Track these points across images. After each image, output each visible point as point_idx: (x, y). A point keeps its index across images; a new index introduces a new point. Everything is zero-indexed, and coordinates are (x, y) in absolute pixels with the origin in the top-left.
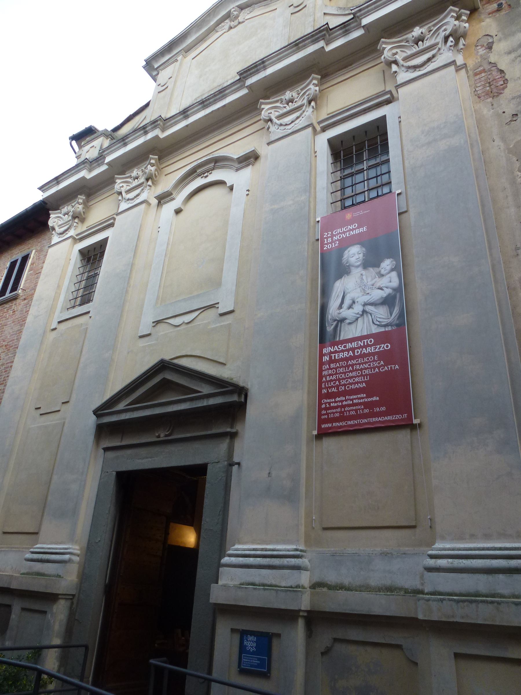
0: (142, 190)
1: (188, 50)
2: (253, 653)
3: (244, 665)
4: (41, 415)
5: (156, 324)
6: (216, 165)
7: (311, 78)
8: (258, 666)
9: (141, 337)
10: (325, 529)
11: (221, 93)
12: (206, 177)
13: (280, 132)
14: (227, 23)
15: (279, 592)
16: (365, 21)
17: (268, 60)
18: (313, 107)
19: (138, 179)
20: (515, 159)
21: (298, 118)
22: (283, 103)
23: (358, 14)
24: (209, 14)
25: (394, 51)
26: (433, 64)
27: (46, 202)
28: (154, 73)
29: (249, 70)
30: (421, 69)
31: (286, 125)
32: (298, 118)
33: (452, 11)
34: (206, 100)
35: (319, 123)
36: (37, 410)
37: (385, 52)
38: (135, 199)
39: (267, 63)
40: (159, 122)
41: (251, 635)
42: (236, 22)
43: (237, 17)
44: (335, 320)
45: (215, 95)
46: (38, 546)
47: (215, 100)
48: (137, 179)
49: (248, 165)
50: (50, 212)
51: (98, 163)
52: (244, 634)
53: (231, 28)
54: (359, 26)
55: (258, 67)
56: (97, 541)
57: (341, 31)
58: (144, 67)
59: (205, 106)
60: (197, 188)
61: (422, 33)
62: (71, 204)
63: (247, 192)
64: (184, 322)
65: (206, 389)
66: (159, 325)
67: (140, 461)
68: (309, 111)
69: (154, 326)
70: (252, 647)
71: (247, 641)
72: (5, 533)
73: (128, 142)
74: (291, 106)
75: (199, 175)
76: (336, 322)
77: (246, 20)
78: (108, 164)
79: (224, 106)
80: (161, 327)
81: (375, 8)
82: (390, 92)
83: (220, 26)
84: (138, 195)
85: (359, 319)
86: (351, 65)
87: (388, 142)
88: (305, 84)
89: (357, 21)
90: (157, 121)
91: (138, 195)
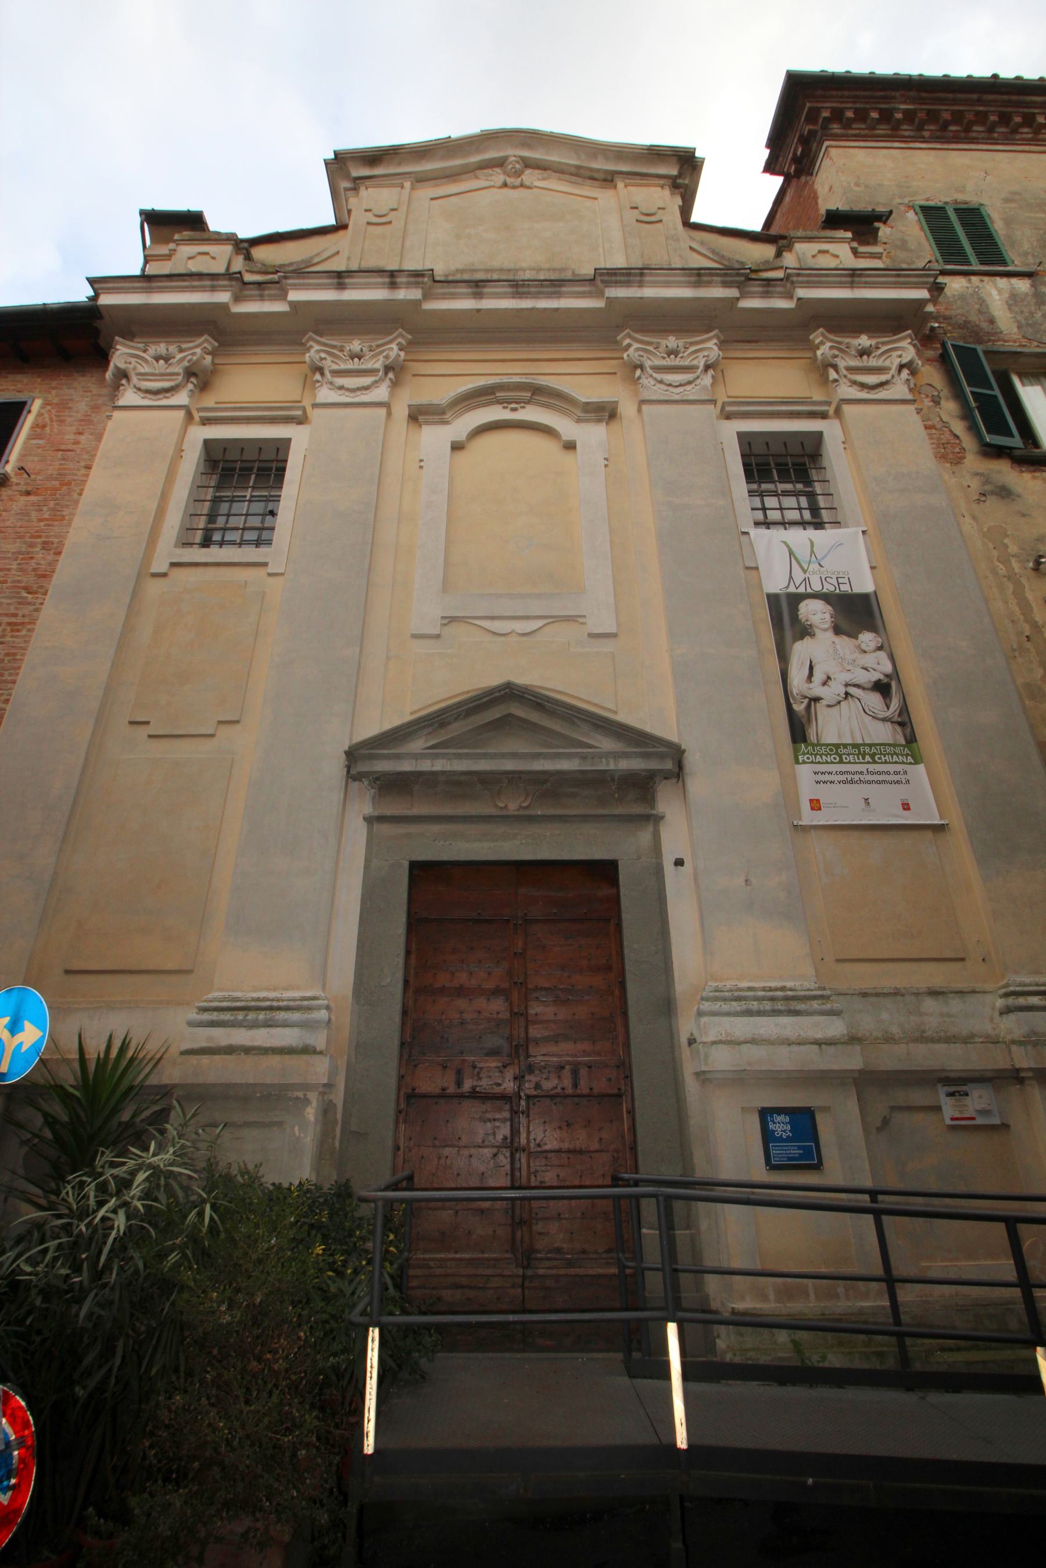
0: (376, 382)
1: (421, 179)
2: (788, 1139)
4: (150, 736)
7: (396, 334)
8: (801, 1157)
14: (498, 177)
16: (802, 293)
19: (362, 360)
21: (689, 383)
23: (795, 279)
24: (471, 142)
28: (345, 184)
31: (670, 385)
32: (689, 383)
33: (401, 335)
37: (312, 351)
38: (359, 393)
39: (647, 278)
41: (779, 1115)
42: (518, 182)
43: (518, 174)
44: (806, 697)
47: (539, 293)
53: (505, 185)
54: (789, 296)
55: (631, 278)
58: (327, 163)
59: (518, 293)
61: (871, 346)
62: (179, 342)
63: (422, 464)
65: (606, 744)
69: (445, 625)
70: (784, 1131)
71: (774, 1123)
75: (499, 402)
76: (806, 701)
77: (536, 187)
78: (294, 305)
79: (556, 310)
80: (458, 630)
81: (808, 282)
83: (486, 171)
84: (366, 388)
85: (842, 703)
88: (699, 338)
91: (366, 388)
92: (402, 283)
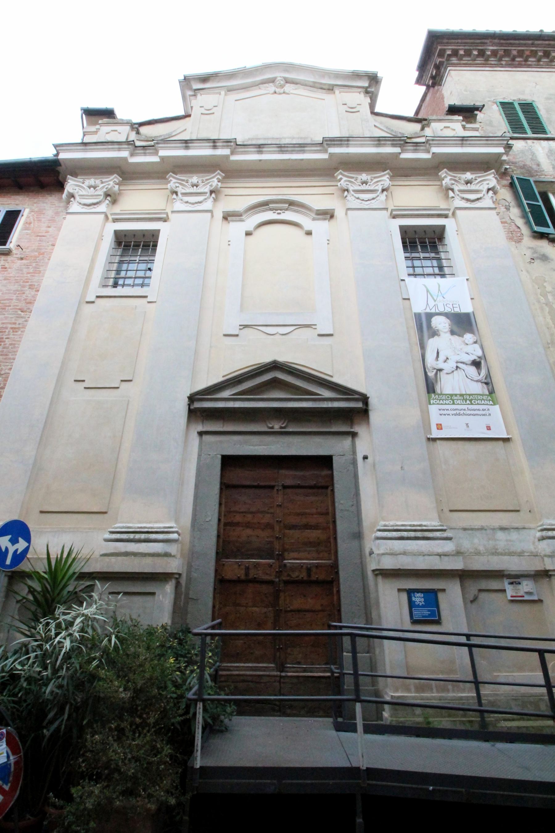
2: (423, 606)
3: (417, 617)
4: (85, 388)
5: (244, 328)
6: (290, 207)
7: (216, 173)
8: (430, 616)
9: (225, 335)
10: (451, 511)
11: (301, 147)
12: (279, 214)
13: (356, 204)
15: (442, 557)
17: (353, 141)
18: (213, 198)
20: (537, 287)
21: (373, 199)
22: (357, 181)
23: (431, 142)
25: (177, 185)
26: (479, 203)
27: (62, 164)
29: (334, 141)
30: (472, 203)
31: (363, 200)
32: (373, 199)
34: (284, 147)
35: (112, 214)
36: (76, 382)
37: (172, 183)
40: (232, 144)
45: (294, 145)
46: (116, 525)
48: (197, 187)
49: (325, 219)
50: (68, 176)
51: (145, 151)
52: (410, 592)
55: (343, 142)
56: (207, 520)
57: (412, 148)
59: (281, 151)
60: (268, 220)
63: (230, 243)
64: (277, 333)
65: (327, 394)
66: (246, 329)
67: (251, 447)
68: (383, 197)
71: (415, 597)
72: (42, 512)
73: (192, 147)
74: (195, 190)
75: (271, 210)
79: (302, 160)
82: (167, 214)
86: (410, 176)
87: (156, 249)
89: (425, 146)
90: (231, 142)
92: (219, 146)
